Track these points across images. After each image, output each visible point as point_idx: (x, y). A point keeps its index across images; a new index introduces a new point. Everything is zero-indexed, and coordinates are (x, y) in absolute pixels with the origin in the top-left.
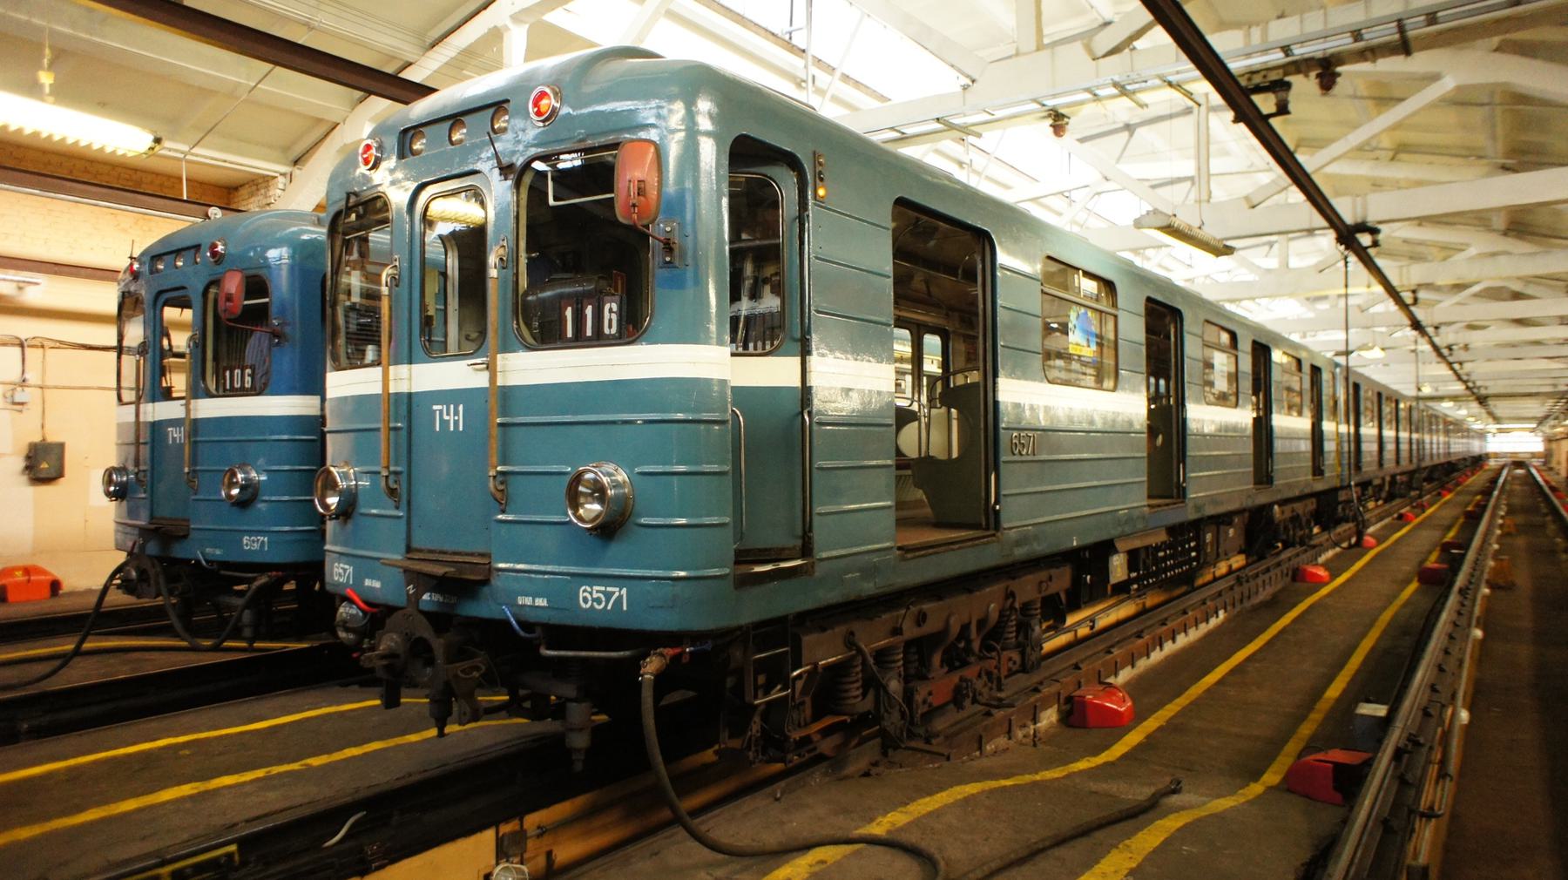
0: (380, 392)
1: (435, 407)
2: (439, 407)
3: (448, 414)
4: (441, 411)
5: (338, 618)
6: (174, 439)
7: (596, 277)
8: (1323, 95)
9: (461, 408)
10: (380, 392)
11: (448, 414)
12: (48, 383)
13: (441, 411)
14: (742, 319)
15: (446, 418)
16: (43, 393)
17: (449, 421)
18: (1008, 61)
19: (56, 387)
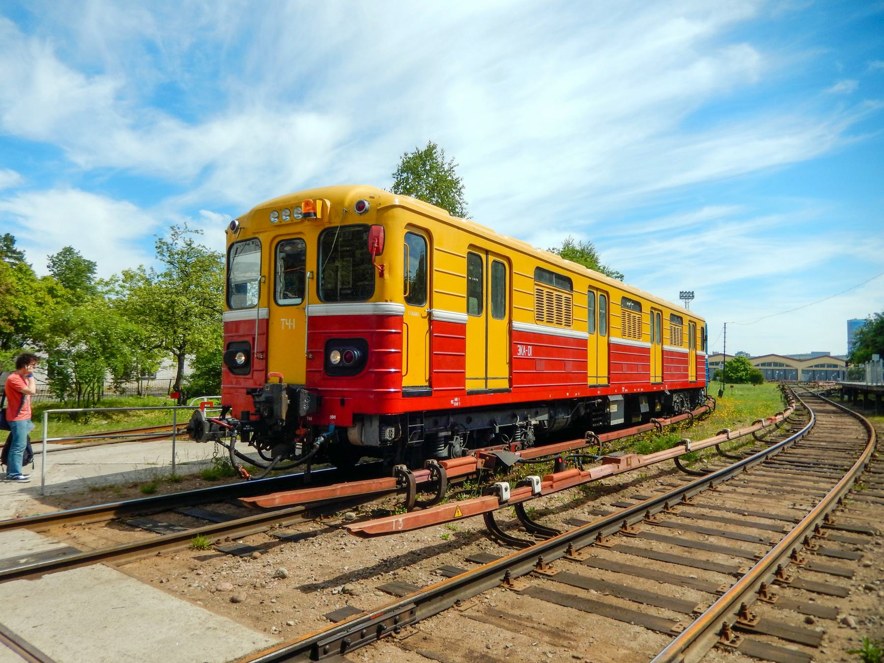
0: (648, 410)
1: (282, 320)
2: (284, 320)
3: (288, 322)
4: (285, 322)
5: (526, 511)
6: (287, 327)
7: (377, 258)
8: (68, 251)
9: (294, 320)
10: (648, 410)
11: (288, 322)
12: (484, 376)
13: (285, 322)
14: (227, 335)
15: (287, 324)
16: (490, 378)
17: (288, 326)
18: (260, 372)
19: (493, 378)
